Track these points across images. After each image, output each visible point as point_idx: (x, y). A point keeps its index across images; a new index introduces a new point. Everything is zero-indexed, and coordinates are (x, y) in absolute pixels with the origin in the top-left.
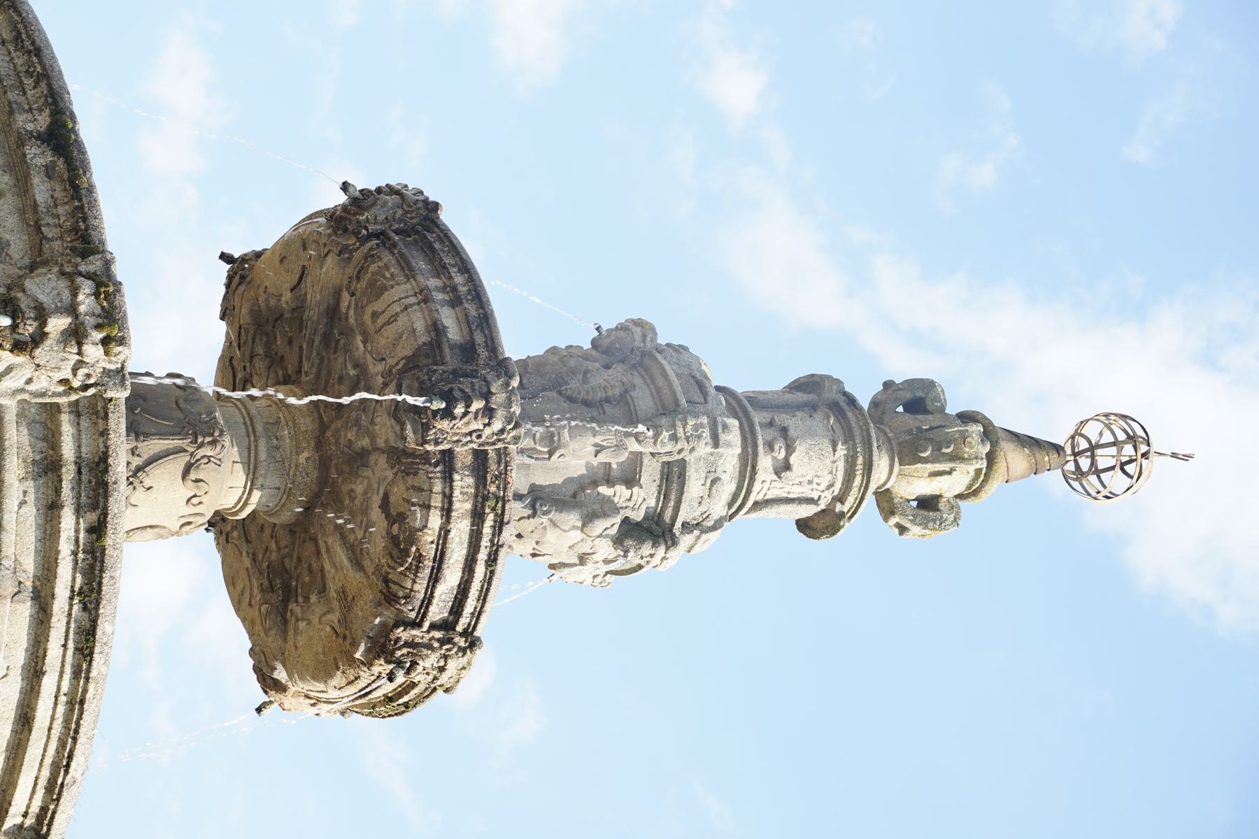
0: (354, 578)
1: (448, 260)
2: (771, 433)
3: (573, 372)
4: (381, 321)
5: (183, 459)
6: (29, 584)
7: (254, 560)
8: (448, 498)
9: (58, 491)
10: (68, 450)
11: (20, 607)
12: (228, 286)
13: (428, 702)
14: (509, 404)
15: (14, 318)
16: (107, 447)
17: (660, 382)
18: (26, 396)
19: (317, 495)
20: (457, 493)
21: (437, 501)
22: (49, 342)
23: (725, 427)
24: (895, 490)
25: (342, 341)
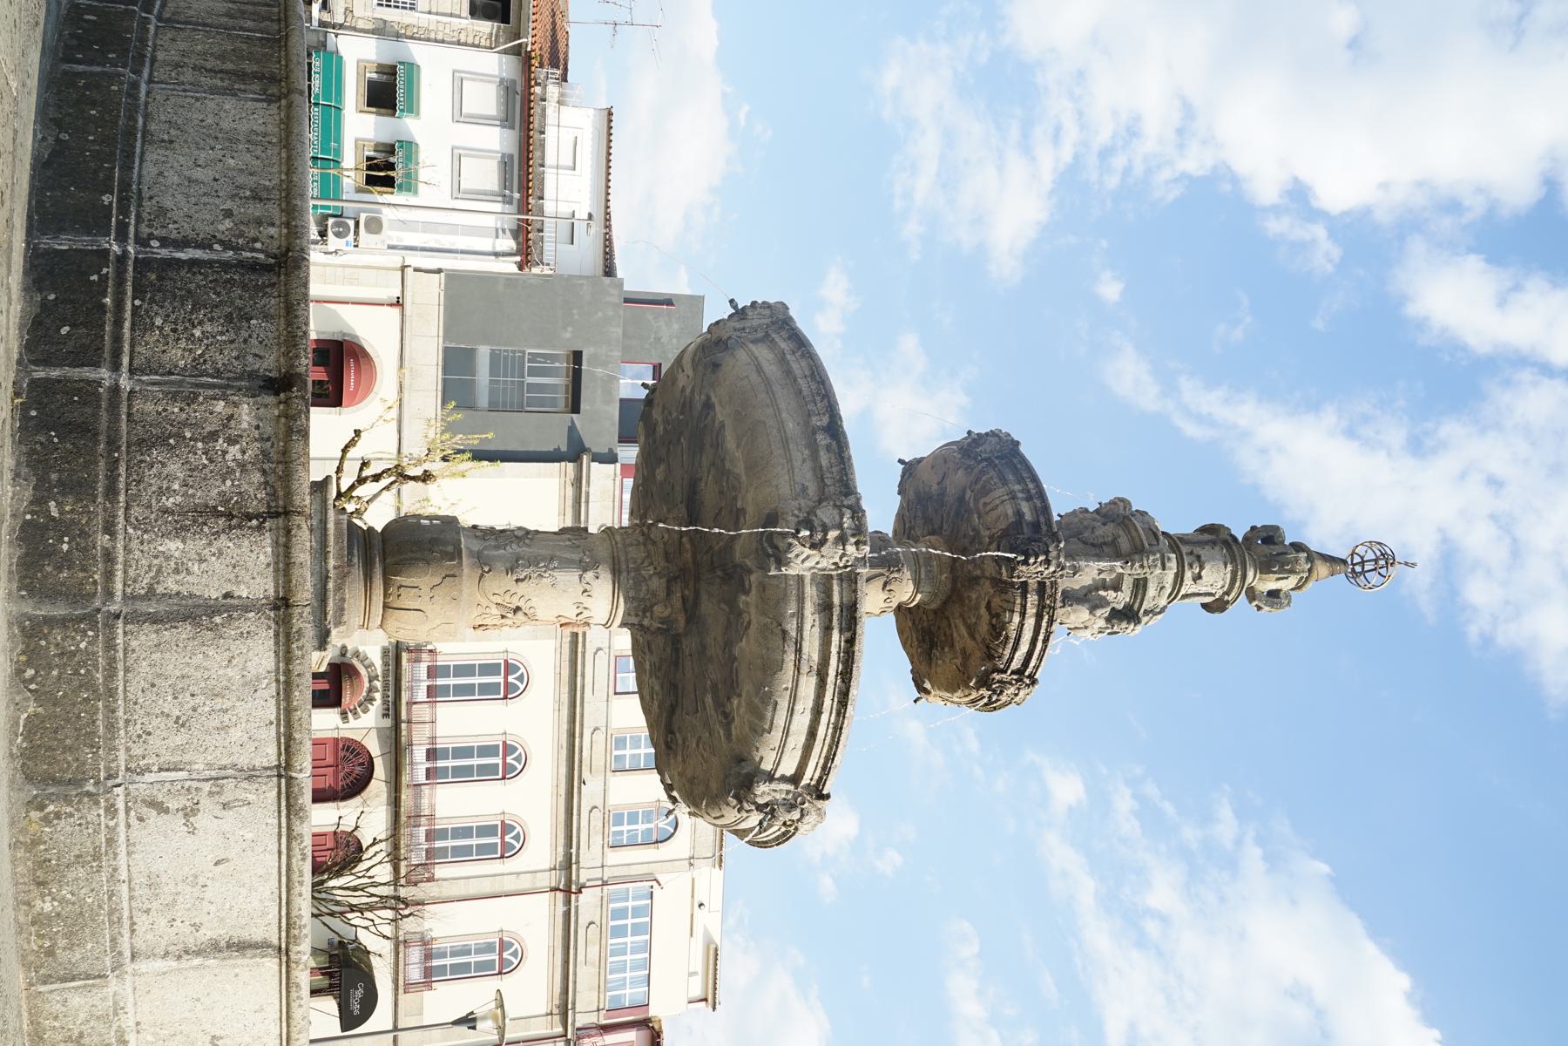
0: (970, 644)
2: (1192, 558)
3: (1086, 528)
4: (988, 508)
5: (883, 579)
6: (815, 667)
7: (914, 623)
8: (1024, 607)
9: (831, 620)
10: (836, 599)
11: (811, 679)
12: (902, 477)
13: (1006, 708)
14: (1058, 557)
15: (811, 531)
16: (856, 599)
17: (1134, 534)
18: (816, 571)
19: (950, 597)
20: (1029, 605)
21: (1018, 608)
22: (828, 544)
23: (1169, 559)
24: (1257, 587)
25: (966, 516)
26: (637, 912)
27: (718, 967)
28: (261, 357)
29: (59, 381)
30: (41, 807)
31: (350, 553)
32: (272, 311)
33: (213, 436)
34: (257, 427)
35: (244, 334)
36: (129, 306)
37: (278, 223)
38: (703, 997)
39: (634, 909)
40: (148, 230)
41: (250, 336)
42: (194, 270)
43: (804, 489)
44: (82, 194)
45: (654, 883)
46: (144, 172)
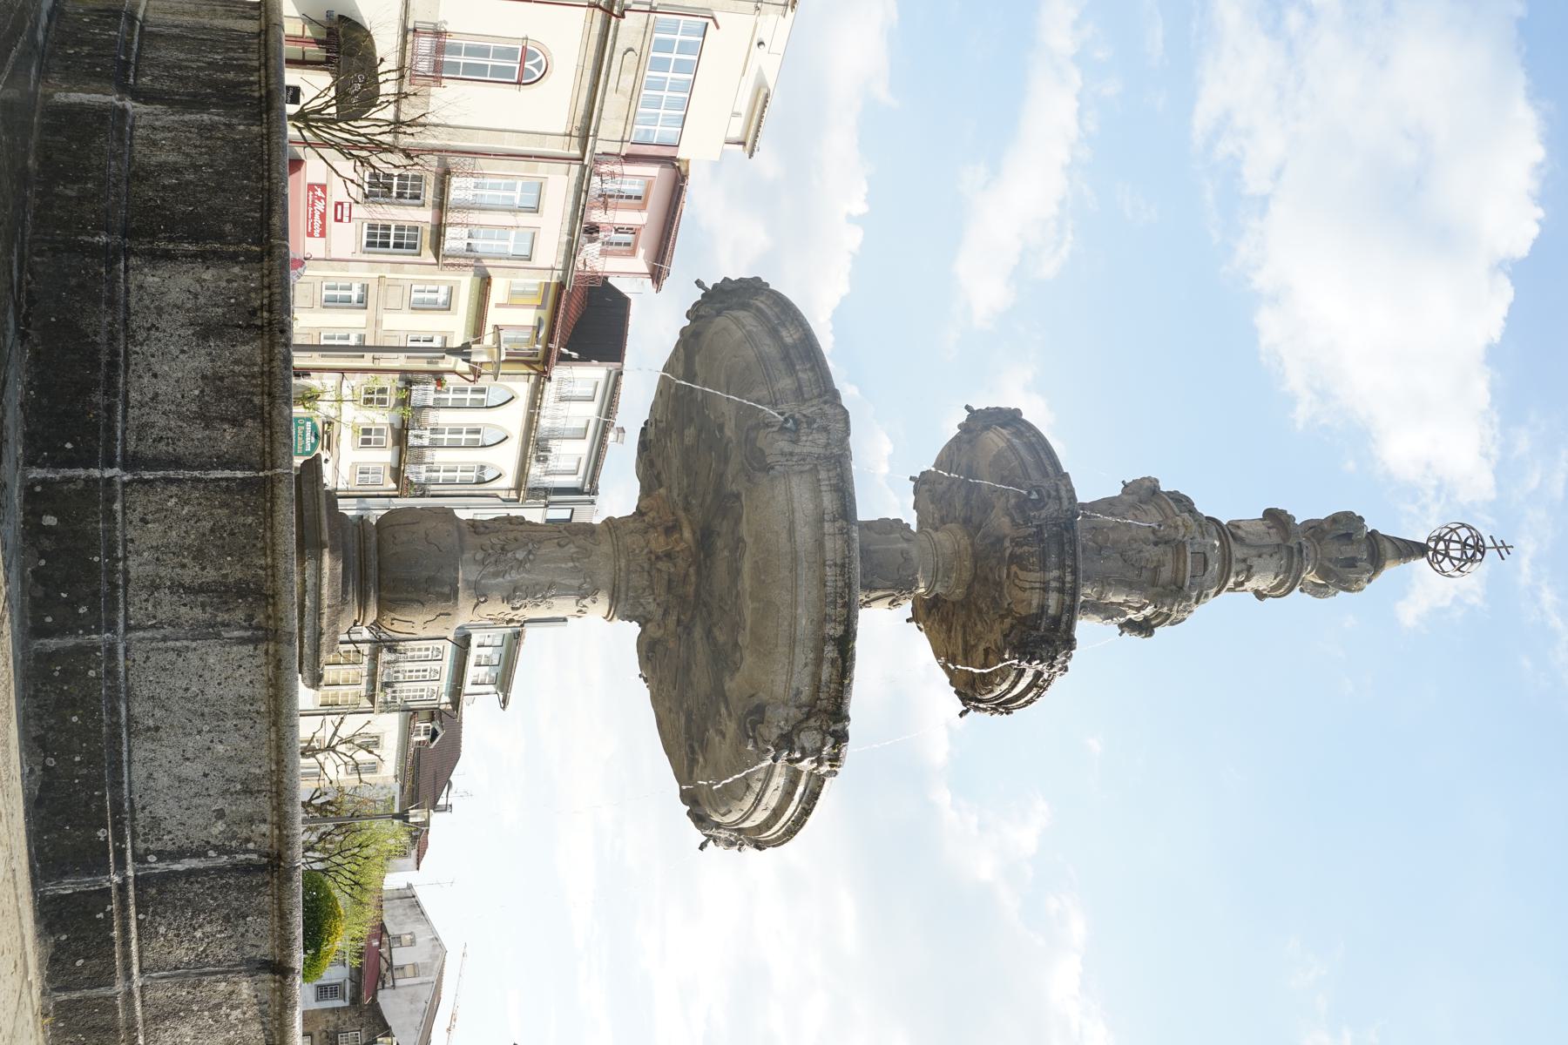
1: (1068, 562)
26: (684, 47)
27: (765, 115)
28: (257, 946)
29: (80, 1001)
31: (345, 592)
32: (266, 907)
33: (218, 1006)
34: (256, 996)
35: (241, 929)
36: (133, 924)
37: (269, 819)
38: (741, 140)
39: (681, 42)
40: (144, 846)
41: (247, 931)
42: (192, 880)
43: (798, 693)
44: (77, 833)
45: (710, 22)
46: (134, 778)
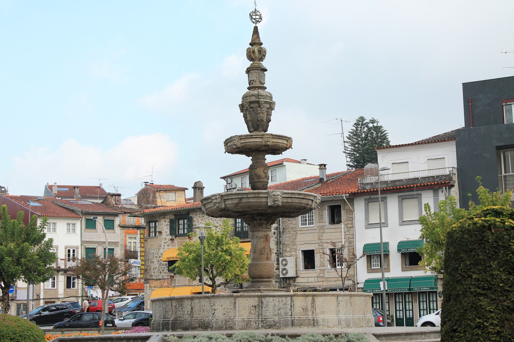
30: (211, 327)
